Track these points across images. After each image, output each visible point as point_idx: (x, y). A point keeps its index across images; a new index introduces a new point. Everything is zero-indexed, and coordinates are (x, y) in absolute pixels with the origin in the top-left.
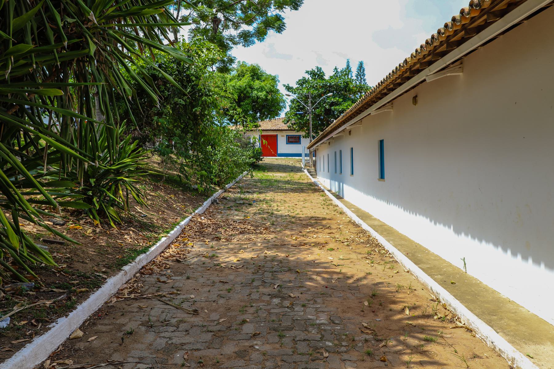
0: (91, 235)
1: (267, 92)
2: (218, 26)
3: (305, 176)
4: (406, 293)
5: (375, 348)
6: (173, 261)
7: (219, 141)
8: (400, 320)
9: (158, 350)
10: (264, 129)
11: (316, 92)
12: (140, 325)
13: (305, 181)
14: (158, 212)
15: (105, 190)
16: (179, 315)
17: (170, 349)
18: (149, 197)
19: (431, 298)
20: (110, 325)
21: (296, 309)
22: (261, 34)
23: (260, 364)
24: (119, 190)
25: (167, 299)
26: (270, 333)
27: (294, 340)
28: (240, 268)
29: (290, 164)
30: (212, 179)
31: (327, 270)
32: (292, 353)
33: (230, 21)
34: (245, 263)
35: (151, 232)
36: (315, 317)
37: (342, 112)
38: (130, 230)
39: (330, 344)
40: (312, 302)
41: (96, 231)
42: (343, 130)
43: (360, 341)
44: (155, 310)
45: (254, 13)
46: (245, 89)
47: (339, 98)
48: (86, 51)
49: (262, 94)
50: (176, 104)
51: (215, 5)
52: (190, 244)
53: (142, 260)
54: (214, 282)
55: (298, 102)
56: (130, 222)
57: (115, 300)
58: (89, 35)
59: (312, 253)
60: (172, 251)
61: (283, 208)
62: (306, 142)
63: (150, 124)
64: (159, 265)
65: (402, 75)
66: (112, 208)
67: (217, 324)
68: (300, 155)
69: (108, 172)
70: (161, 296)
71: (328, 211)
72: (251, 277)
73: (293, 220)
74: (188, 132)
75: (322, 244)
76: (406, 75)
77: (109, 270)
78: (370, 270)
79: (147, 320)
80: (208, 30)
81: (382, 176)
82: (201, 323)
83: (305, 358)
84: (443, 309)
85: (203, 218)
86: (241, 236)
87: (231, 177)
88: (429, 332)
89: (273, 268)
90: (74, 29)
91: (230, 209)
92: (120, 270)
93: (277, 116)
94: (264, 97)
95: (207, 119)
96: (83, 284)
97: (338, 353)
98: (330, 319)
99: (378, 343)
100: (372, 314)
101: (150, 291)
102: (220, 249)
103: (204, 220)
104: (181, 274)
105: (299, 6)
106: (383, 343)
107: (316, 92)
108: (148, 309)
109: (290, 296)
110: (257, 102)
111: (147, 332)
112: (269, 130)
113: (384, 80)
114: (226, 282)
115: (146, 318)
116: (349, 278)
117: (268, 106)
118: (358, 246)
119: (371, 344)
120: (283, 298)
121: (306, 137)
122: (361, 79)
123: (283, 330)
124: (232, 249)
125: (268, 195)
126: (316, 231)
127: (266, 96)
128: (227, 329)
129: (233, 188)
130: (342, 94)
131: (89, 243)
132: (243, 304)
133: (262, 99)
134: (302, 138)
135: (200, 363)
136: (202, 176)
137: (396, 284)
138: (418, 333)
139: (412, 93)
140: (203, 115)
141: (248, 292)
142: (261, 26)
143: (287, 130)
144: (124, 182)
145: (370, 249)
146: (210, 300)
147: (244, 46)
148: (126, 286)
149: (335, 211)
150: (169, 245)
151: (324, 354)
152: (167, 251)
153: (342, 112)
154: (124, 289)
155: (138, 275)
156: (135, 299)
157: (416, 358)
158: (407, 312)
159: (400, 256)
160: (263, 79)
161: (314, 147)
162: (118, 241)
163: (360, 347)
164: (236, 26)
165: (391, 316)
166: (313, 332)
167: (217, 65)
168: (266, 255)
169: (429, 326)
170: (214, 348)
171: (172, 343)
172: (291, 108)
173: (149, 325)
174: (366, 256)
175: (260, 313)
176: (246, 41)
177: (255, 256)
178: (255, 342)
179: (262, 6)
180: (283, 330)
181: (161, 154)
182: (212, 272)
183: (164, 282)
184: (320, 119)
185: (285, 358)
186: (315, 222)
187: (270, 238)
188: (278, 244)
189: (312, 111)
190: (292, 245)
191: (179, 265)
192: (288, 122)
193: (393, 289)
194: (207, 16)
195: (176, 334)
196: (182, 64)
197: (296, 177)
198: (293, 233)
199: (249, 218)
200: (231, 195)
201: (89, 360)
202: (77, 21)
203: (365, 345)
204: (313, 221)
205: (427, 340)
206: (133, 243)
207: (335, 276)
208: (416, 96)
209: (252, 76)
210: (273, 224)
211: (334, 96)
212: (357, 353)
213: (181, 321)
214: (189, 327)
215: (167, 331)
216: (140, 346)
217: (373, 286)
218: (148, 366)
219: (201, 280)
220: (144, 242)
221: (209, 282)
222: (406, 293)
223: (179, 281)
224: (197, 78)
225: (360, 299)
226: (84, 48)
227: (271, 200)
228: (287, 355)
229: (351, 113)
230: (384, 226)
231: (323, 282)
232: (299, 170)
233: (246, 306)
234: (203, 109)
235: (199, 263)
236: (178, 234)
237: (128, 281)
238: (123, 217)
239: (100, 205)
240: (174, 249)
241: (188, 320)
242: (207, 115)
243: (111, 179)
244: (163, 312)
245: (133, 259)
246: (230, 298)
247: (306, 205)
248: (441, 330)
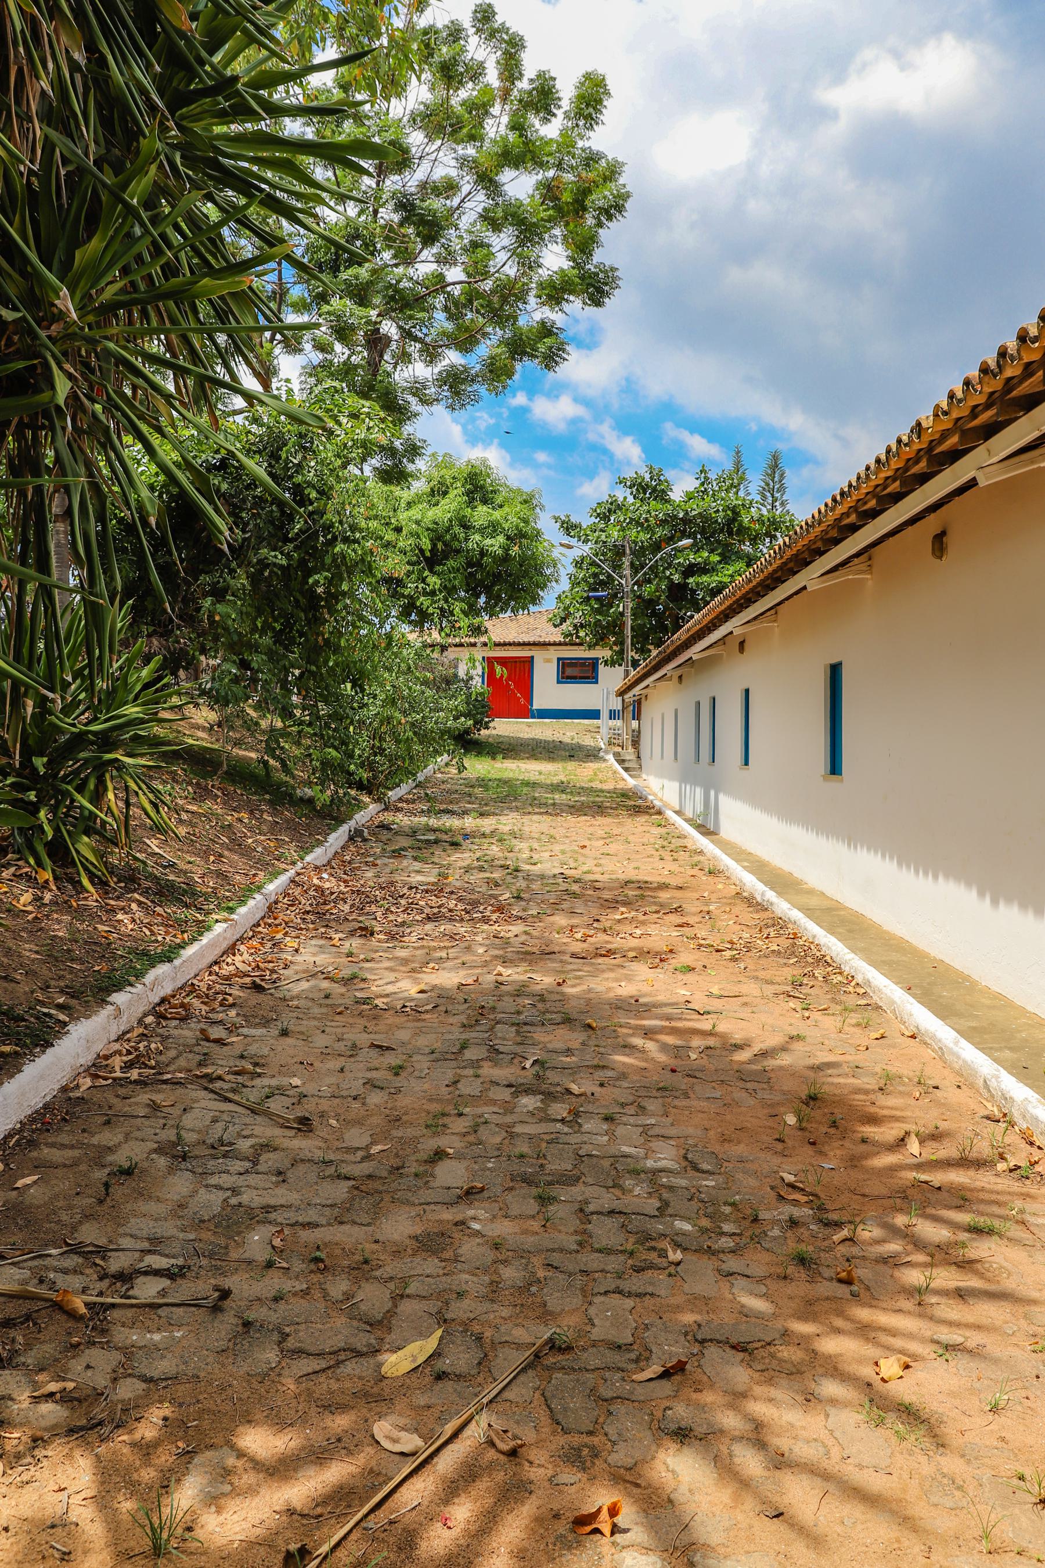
0: (30, 908)
1: (508, 538)
2: (381, 356)
3: (607, 773)
4: (909, 1094)
5: (819, 1243)
6: (243, 987)
7: (375, 668)
8: (893, 1169)
9: (203, 1221)
10: (496, 639)
11: (644, 537)
12: (155, 1151)
13: (609, 786)
14: (205, 854)
15: (69, 788)
16: (258, 1130)
17: (235, 1219)
18: (184, 816)
19: (986, 1113)
20: (72, 1147)
21: (587, 1127)
22: (497, 373)
23: (486, 1272)
24: (106, 789)
25: (226, 1086)
26: (511, 1189)
27: (581, 1210)
28: (427, 1011)
29: (567, 740)
30: (351, 774)
31: (674, 1024)
32: (575, 1247)
33: (416, 339)
34: (442, 1001)
35: (187, 906)
36: (641, 1152)
37: (715, 592)
38: (131, 900)
39: (687, 1227)
40: (631, 1110)
41: (42, 898)
42: (723, 640)
43: (775, 1222)
44: (196, 1113)
45: (481, 319)
46: (448, 530)
47: (712, 551)
48: (45, 396)
49: (495, 544)
50: (263, 564)
51: (377, 300)
52: (290, 943)
53: (161, 980)
54: (354, 1046)
55: (593, 564)
56: (131, 879)
57: (88, 1082)
58: (54, 356)
59: (629, 978)
60: (242, 960)
61: (547, 855)
62: (612, 678)
63: (190, 618)
64: (207, 996)
65: (906, 469)
66: (86, 839)
67: (364, 1159)
68: (594, 714)
69: (79, 740)
70: (210, 1078)
71: (675, 867)
72: (457, 1035)
73: (575, 887)
74: (292, 642)
75: (657, 953)
76: (916, 469)
77: (73, 1002)
78: (799, 1027)
79: (174, 1138)
80: (356, 367)
81: (835, 768)
82: (318, 1154)
83: (614, 1263)
84: (1023, 1145)
85: (325, 876)
86: (429, 927)
87: (402, 767)
88: (982, 1207)
89: (519, 1013)
90: (16, 338)
91: (400, 856)
92: (104, 1002)
93: (535, 604)
94: (500, 552)
95: (346, 607)
96: (6, 1035)
97: (711, 1252)
98: (685, 1158)
99: (828, 1231)
100: (809, 1150)
101: (182, 1062)
102: (372, 960)
103: (329, 884)
104: (266, 1023)
105: (608, 295)
106: (845, 1233)
107: (644, 537)
108: (176, 1111)
109: (568, 1091)
110: (479, 564)
111: (171, 1170)
112: (510, 644)
113: (850, 485)
114: (388, 1048)
115: (170, 1135)
116: (738, 1047)
117: (505, 579)
118: (763, 961)
119: (806, 1233)
120: (549, 1096)
121: (613, 664)
122: (775, 500)
123: (550, 1183)
124: (405, 961)
125: (503, 819)
126: (642, 918)
127: (507, 550)
128: (390, 1173)
129: (407, 801)
130: (719, 542)
131: (24, 929)
132: (435, 1107)
133: (495, 557)
134: (601, 667)
135: (317, 1260)
136: (326, 764)
137: (878, 1069)
138: (949, 1207)
139: (932, 524)
140: (333, 596)
141: (450, 1076)
142: (499, 351)
143: (560, 644)
144: (119, 766)
145: (797, 971)
146: (344, 1093)
147: (452, 408)
148: (117, 1046)
149: (693, 866)
150: (235, 944)
151: (670, 1253)
152: (229, 960)
153: (715, 592)
154: (111, 1055)
155: (150, 1019)
156: (141, 1083)
157: (946, 1278)
158: (914, 1146)
159: (887, 989)
160: (499, 500)
161: (636, 690)
162: (100, 927)
163: (775, 1238)
164: (431, 354)
165: (866, 1156)
166: (637, 1191)
167: (374, 461)
168: (500, 979)
169: (983, 1189)
170: (355, 1223)
171: (240, 1205)
172: (575, 583)
173: (178, 1154)
174: (789, 988)
175: (484, 1133)
176: (456, 393)
177: (470, 981)
178: (471, 1213)
179: (504, 299)
180: (550, 1183)
181: (217, 699)
182: (351, 1020)
183: (219, 1041)
184: (654, 614)
185: (556, 1258)
186: (635, 895)
187: (510, 934)
188: (535, 950)
189: (633, 591)
190: (574, 955)
191: (261, 998)
192: (563, 620)
193: (871, 1083)
194: (353, 329)
195: (252, 1179)
196: (284, 456)
197: (582, 773)
198: (575, 921)
199: (450, 879)
200: (402, 820)
201: (18, 1238)
202: (23, 318)
203: (789, 1234)
204: (631, 893)
205: (977, 1231)
206: (140, 935)
207: (697, 1042)
208: (943, 533)
209: (468, 493)
210: (519, 898)
211: (696, 548)
212: (766, 1257)
213: (267, 1147)
214: (287, 1163)
215: (228, 1172)
216: (152, 1207)
217: (811, 1074)
218: (173, 1261)
219: (321, 1041)
220: (167, 933)
221: (340, 1046)
222: (909, 1094)
223: (261, 1040)
224: (321, 493)
225: (772, 1106)
226: (38, 391)
227: (513, 834)
228: (561, 1250)
229: (747, 588)
230: (837, 909)
231: (662, 1058)
232: (592, 755)
233: (444, 1115)
234: (334, 581)
235: (316, 995)
236: (258, 916)
237: (124, 1033)
238: (113, 866)
239: (57, 830)
240: (246, 956)
241: (285, 1146)
242: (344, 594)
243: (87, 760)
244: (215, 1121)
245: (139, 975)
246: (398, 1090)
247: (613, 848)
248: (1018, 1204)
